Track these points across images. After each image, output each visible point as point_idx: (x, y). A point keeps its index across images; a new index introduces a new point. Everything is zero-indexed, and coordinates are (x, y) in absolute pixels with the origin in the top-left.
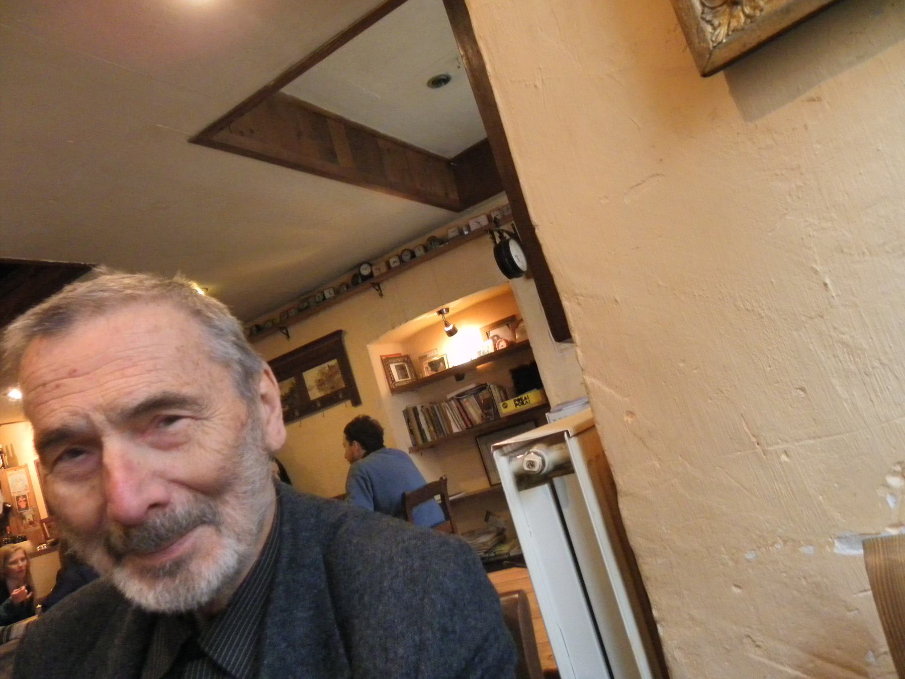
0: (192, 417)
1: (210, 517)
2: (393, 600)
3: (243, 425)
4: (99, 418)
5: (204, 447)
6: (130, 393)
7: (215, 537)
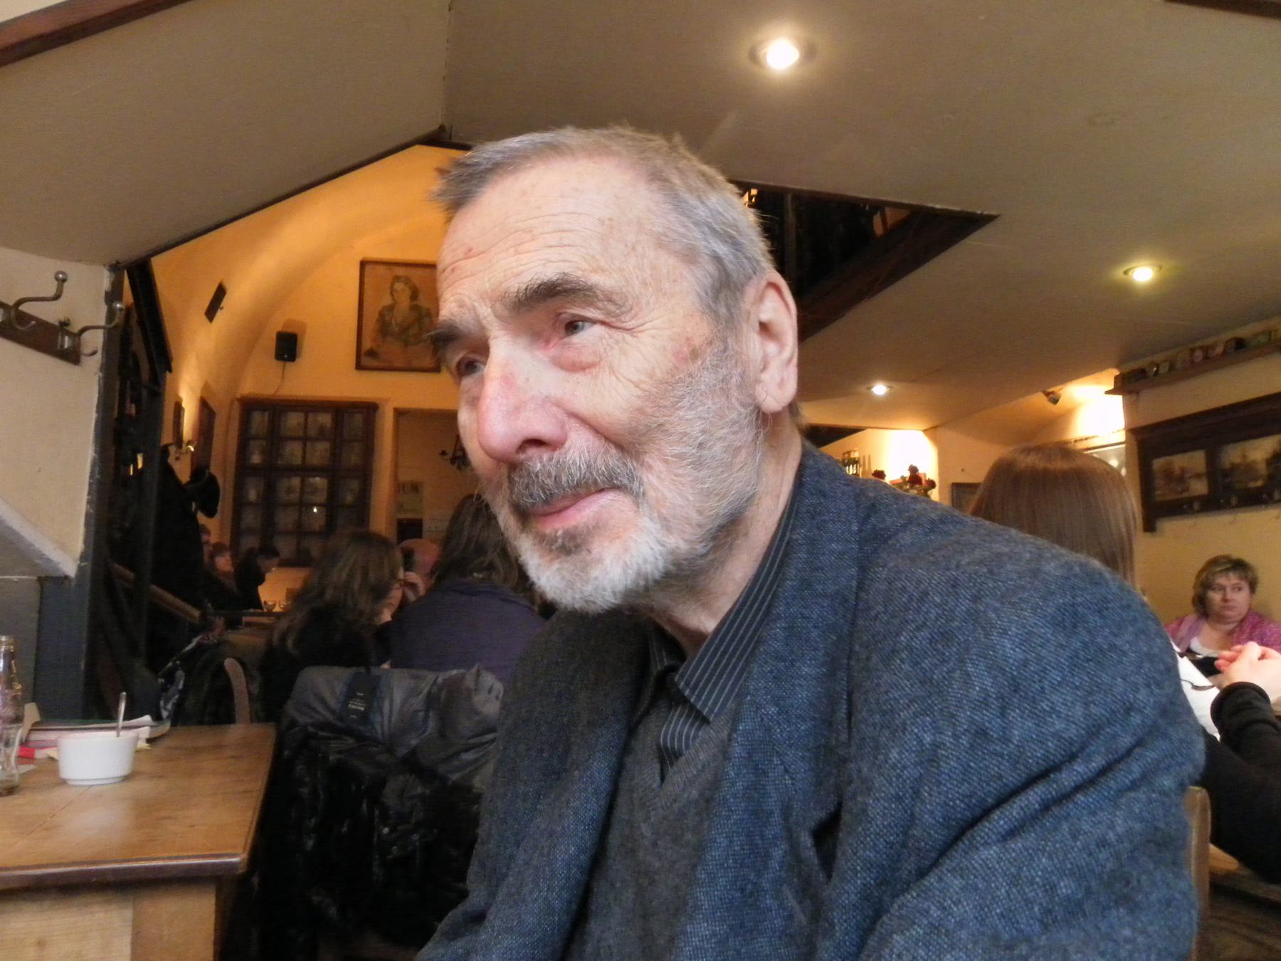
0: (603, 323)
1: (626, 481)
2: (906, 667)
3: (695, 354)
4: (485, 312)
5: (618, 374)
6: (518, 274)
7: (631, 514)
